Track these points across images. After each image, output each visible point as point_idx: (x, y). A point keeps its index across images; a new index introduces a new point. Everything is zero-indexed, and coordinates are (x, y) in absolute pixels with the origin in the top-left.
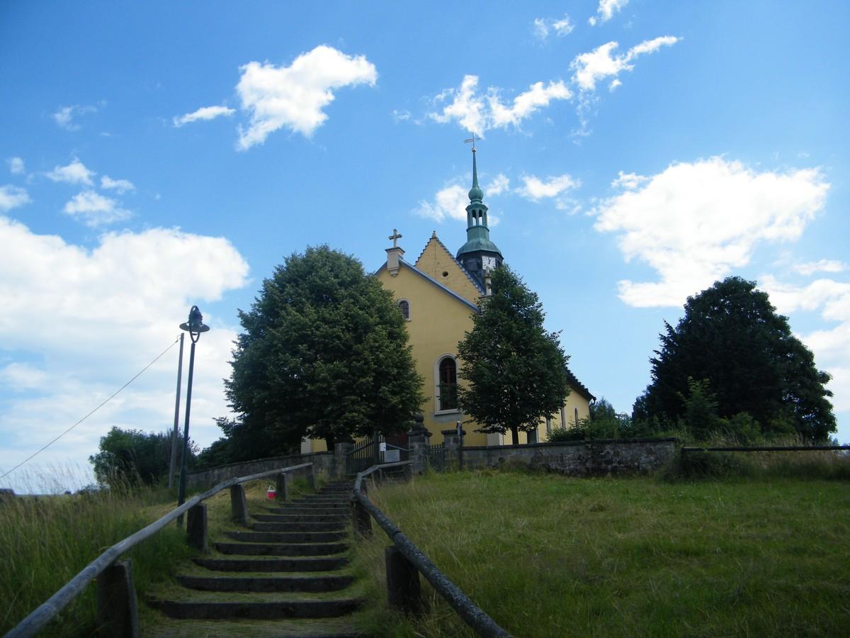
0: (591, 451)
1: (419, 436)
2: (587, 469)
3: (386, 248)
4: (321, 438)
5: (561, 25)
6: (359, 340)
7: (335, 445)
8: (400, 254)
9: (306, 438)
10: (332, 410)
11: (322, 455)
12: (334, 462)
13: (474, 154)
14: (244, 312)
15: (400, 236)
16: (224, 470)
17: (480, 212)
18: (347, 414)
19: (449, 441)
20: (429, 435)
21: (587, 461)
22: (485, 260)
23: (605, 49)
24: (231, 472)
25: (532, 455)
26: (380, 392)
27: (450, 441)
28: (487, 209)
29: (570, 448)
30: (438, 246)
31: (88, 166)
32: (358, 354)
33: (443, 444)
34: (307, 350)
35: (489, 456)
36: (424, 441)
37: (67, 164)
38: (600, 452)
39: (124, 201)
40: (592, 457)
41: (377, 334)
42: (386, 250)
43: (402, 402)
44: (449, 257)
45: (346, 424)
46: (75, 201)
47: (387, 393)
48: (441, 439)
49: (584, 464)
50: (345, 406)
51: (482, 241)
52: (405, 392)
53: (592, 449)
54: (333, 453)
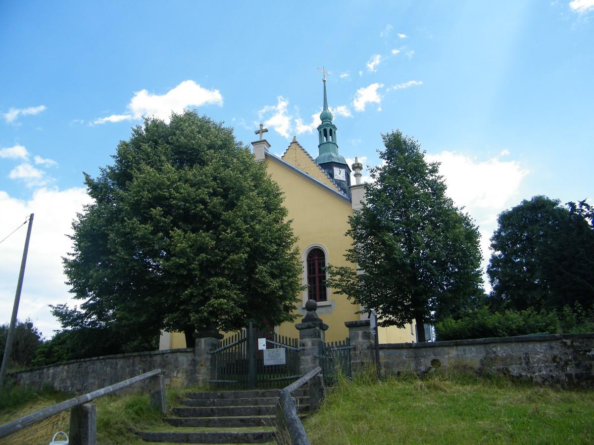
0: (571, 350)
1: (312, 330)
2: (569, 376)
3: (253, 141)
4: (180, 331)
5: (344, 75)
6: (231, 206)
7: (197, 340)
8: (266, 147)
9: (162, 331)
10: (191, 294)
11: (178, 354)
12: (194, 363)
13: (324, 83)
14: (92, 178)
15: (266, 131)
16: (59, 369)
17: (331, 130)
18: (212, 301)
19: (357, 335)
20: (324, 327)
21: (566, 364)
22: (336, 170)
23: (374, 87)
24: (68, 372)
25: (481, 356)
26: (257, 274)
27: (358, 337)
28: (336, 129)
29: (538, 345)
30: (299, 149)
31: (28, 149)
32: (227, 223)
33: (348, 340)
34: (163, 216)
35: (416, 357)
36: (319, 336)
37: (12, 146)
38: (586, 351)
39: (49, 172)
40: (575, 359)
41: (252, 200)
42: (252, 143)
43: (282, 287)
44: (309, 159)
45: (211, 313)
46: (17, 170)
47: (264, 274)
48: (345, 333)
49: (563, 369)
50: (210, 290)
51: (333, 155)
52: (286, 275)
53: (572, 346)
54: (194, 352)
